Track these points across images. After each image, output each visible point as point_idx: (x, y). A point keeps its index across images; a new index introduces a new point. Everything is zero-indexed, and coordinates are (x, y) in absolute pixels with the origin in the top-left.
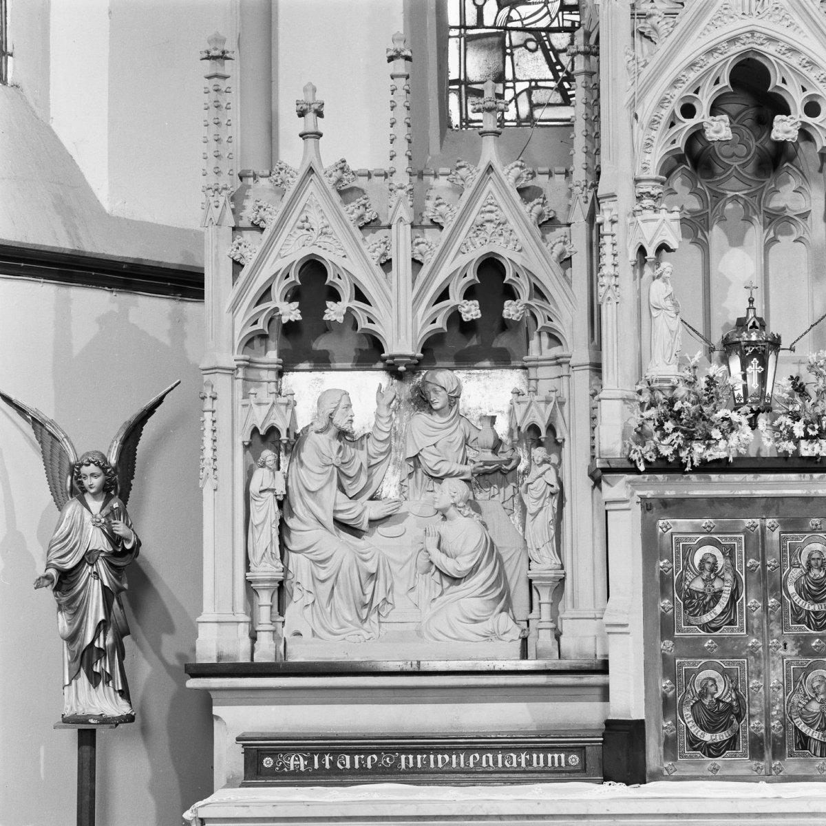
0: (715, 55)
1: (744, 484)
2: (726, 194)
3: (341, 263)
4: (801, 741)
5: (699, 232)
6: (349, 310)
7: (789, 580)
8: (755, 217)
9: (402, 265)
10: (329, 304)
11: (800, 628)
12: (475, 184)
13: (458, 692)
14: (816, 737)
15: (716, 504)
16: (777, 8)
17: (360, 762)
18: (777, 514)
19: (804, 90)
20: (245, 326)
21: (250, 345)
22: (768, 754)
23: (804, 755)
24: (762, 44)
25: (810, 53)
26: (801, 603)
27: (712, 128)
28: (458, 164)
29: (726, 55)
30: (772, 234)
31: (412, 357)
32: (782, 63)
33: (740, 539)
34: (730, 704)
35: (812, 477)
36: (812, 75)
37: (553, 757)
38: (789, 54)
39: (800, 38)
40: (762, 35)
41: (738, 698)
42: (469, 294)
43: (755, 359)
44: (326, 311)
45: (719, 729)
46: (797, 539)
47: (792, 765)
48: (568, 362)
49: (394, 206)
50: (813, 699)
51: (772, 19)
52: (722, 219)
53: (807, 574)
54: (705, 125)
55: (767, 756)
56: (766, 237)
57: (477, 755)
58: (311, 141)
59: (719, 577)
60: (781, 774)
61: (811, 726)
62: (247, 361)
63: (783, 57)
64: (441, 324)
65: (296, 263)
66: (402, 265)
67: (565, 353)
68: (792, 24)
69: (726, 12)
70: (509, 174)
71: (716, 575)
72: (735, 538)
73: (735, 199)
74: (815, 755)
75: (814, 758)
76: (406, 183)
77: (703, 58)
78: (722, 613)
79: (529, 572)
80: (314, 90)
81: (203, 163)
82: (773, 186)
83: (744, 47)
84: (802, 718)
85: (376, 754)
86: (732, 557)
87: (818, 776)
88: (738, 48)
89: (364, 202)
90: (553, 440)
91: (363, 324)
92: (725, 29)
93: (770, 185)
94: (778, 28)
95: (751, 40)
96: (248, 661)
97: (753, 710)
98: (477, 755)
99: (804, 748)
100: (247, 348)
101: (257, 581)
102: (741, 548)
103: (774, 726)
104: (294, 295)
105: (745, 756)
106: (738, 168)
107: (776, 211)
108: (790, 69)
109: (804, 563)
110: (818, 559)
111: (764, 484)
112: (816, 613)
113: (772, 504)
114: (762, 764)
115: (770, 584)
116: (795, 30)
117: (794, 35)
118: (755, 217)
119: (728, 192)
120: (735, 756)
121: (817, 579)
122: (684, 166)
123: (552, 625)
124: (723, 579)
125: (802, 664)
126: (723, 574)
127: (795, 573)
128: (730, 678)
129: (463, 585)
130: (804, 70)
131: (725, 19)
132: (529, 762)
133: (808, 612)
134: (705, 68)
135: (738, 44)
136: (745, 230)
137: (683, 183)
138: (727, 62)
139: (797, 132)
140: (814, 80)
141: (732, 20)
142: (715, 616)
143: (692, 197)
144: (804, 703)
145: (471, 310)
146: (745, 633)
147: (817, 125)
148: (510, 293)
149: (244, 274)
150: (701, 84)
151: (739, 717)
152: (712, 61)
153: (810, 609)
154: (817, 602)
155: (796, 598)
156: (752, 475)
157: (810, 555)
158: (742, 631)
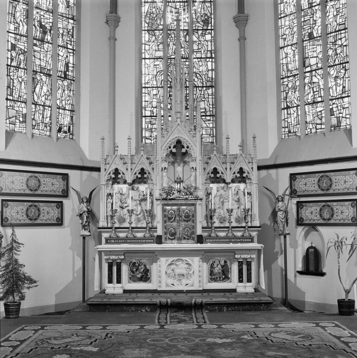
3: (246, 168)
36: (187, 143)
42: (238, 173)
64: (234, 177)
66: (129, 169)
88: (177, 139)
91: (222, 177)
127: (184, 214)
145: (212, 176)
149: (232, 170)
151: (176, 235)
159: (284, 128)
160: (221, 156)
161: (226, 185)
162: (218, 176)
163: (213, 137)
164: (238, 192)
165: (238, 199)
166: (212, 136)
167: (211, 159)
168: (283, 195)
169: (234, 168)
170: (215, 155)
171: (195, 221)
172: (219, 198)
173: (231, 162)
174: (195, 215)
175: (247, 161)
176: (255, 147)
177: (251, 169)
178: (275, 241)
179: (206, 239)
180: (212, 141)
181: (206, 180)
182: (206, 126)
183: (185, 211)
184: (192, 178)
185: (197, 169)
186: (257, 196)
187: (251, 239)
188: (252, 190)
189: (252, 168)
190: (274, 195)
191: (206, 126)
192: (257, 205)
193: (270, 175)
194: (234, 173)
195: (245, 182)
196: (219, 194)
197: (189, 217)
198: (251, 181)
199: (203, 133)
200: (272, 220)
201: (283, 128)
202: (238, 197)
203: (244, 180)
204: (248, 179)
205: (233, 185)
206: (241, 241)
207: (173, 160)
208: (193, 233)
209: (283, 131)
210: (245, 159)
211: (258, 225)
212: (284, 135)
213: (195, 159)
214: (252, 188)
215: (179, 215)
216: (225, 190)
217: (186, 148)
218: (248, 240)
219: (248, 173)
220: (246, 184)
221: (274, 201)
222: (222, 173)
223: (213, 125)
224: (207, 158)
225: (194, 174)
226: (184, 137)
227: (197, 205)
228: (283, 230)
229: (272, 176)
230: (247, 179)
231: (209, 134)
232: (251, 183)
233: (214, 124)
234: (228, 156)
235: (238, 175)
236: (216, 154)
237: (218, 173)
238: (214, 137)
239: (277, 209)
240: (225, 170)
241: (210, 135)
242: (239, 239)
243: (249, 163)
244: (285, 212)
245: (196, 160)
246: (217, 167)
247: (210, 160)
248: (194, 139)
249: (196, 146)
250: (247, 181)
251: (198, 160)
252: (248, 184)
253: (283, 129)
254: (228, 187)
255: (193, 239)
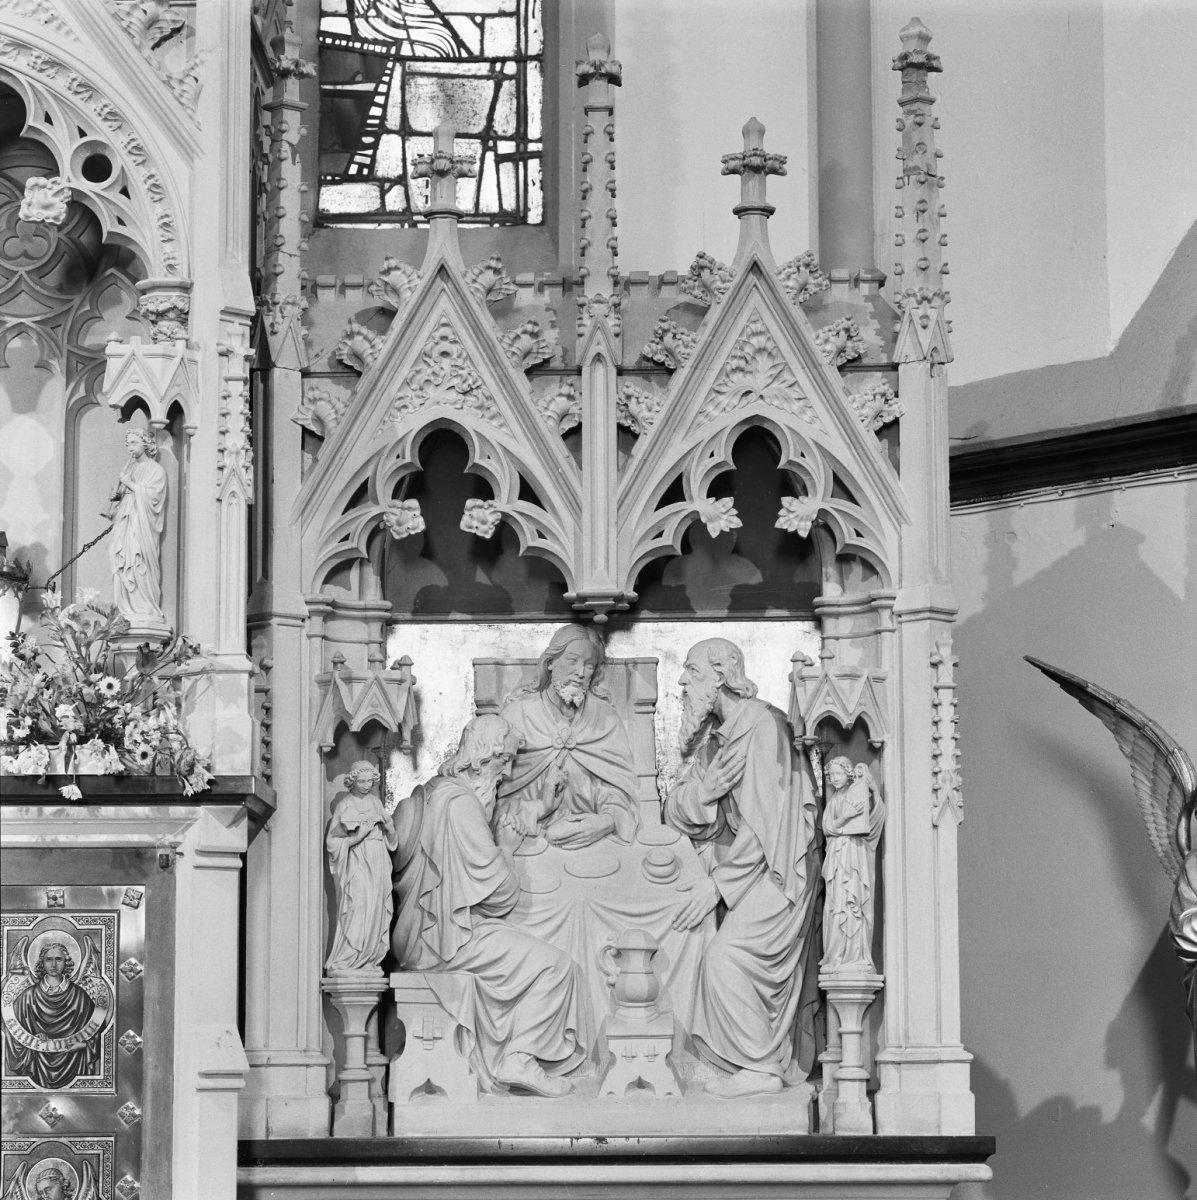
2: (5, 322)
3: (809, 433)
6: (822, 512)
8: (54, 362)
9: (600, 439)
10: (786, 501)
11: (20, 1083)
19: (82, 134)
21: (339, 578)
25: (82, 68)
26: (23, 1037)
28: (385, 266)
30: (82, 392)
31: (619, 598)
35: (40, 813)
36: (90, 109)
38: (51, 71)
39: (66, 43)
42: (717, 489)
46: (23, 923)
48: (891, 607)
49: (587, 335)
51: (19, 10)
53: (37, 985)
62: (328, 604)
64: (671, 539)
65: (728, 430)
66: (600, 439)
67: (885, 592)
68: (53, 18)
73: (20, 330)
80: (761, 132)
82: (88, 308)
89: (847, 324)
91: (528, 539)
93: (81, 305)
96: (324, 1135)
100: (328, 586)
104: (411, 486)
106: (26, 276)
107: (92, 351)
108: (55, 97)
109: (32, 967)
112: (50, 1056)
118: (54, 362)
119: (6, 318)
123: (864, 1074)
125: (20, 1148)
127: (15, 985)
129: (519, 1007)
130: (76, 100)
133: (35, 1055)
136: (41, 385)
140: (93, 115)
145: (409, 519)
148: (791, 484)
149: (640, 448)
153: (40, 1050)
154: (52, 1036)
157: (43, 952)
161: (578, 642)
162: (478, 519)
163: (520, 157)
164: (715, 717)
165: (723, 801)
166: (506, 147)
167: (398, 323)
169: (671, 421)
170: (442, 271)
171: (151, 1075)
172: (484, 786)
173: (631, 361)
174: (151, 990)
175: (824, 344)
176: (930, 179)
180: (509, 204)
182: (447, 46)
184: (134, 534)
185: (192, 418)
189: (889, 430)
191: (447, 46)
193: (1128, 539)
194: (675, 493)
195: (805, 605)
196: (491, 737)
197: (81, 1019)
198: (872, 588)
199: (416, 124)
200: (1140, 1054)
202: (715, 779)
203: (800, 576)
205: (666, 644)
211: (960, 1122)
213: (174, 298)
214: (887, 668)
216: (568, 692)
219: (842, 487)
220: (818, 622)
222: (528, 492)
225: (149, 479)
226: (49, 32)
227: (183, 869)
229: (1145, 553)
230: (830, 570)
231: (479, 126)
235: (722, 517)
236: (456, 265)
238: (534, 165)
240: (560, 449)
243: (851, 365)
245: (183, 317)
246: (468, 420)
247: (383, 331)
248: (174, 57)
249: (188, 151)
251: (205, 323)
254: (599, 662)
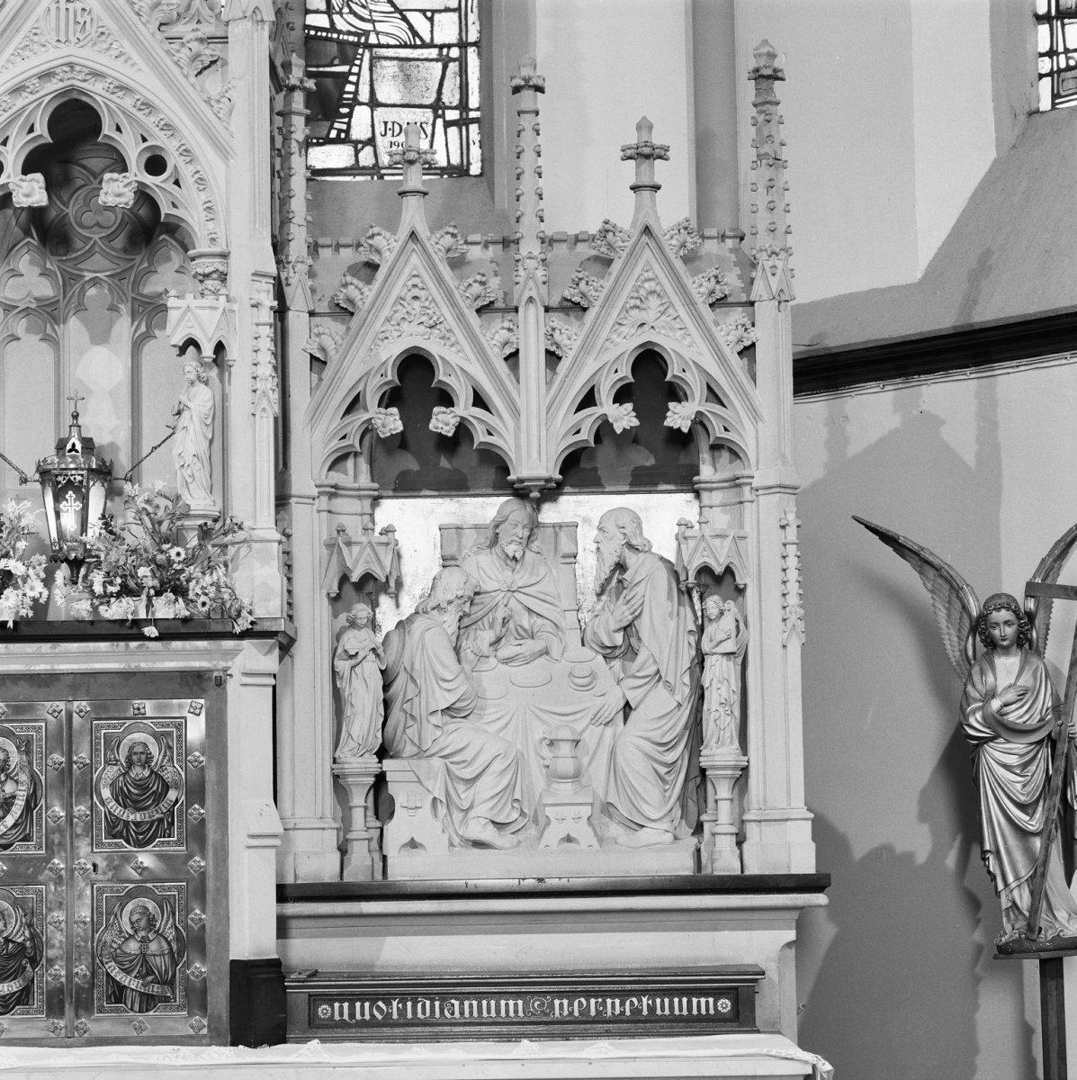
0: (24, 94)
1: (41, 657)
4: (114, 992)
5: (48, 326)
7: (103, 782)
8: (122, 306)
9: (533, 360)
10: (672, 405)
11: (116, 844)
12: (392, 259)
13: (710, 915)
14: (133, 987)
15: (8, 683)
16: (103, 33)
17: (597, 1009)
18: (87, 695)
20: (566, 434)
22: (69, 1010)
23: (117, 1010)
24: (85, 81)
27: (21, 191)
29: (38, 95)
30: (143, 328)
31: (548, 480)
32: (112, 106)
33: (40, 728)
34: (22, 945)
35: (127, 646)
36: (150, 121)
37: (699, 1002)
38: (120, 94)
40: (84, 69)
41: (33, 937)
42: (621, 396)
43: (70, 492)
44: (669, 414)
45: (8, 976)
47: (97, 1024)
50: (131, 936)
51: (96, 48)
52: (81, 308)
53: (127, 773)
54: (11, 187)
55: (67, 1012)
56: (136, 331)
57: (634, 1000)
58: (646, 194)
59: (12, 779)
60: (86, 1035)
61: (128, 972)
62: (332, 487)
63: (113, 97)
64: (586, 435)
66: (533, 360)
67: (746, 473)
68: (122, 54)
69: (36, 38)
70: (440, 244)
71: (8, 776)
72: (34, 727)
74: (132, 1009)
75: (132, 1013)
76: (536, 252)
77: (5, 98)
78: (15, 826)
79: (334, 766)
80: (650, 128)
81: (789, 219)
83: (61, 85)
84: (116, 962)
85: (457, 999)
86: (28, 752)
87: (134, 1037)
88: (54, 86)
90: (733, 587)
91: (480, 437)
92: (34, 61)
93: (141, 263)
94: (103, 59)
95: (70, 75)
96: (337, 880)
97: (51, 953)
98: (583, 1000)
99: (118, 1001)
101: (714, 768)
102: (40, 740)
103: (77, 973)
104: (391, 398)
105: (41, 1012)
107: (149, 297)
110: (142, 753)
111: (66, 657)
112: (137, 824)
113: (80, 683)
114: (62, 1023)
115: (74, 783)
116: (126, 61)
117: (126, 69)
118: (122, 306)
120: (28, 1013)
121: (140, 780)
122: (29, 239)
124: (17, 782)
125: (118, 891)
126: (17, 774)
127: (112, 772)
128: (23, 910)
130: (140, 115)
131: (36, 47)
132: (402, 1012)
133: (126, 823)
134: (11, 112)
135: (55, 81)
136: (111, 324)
137: (32, 262)
138: (41, 103)
139: (132, 195)
140: (153, 127)
141: (43, 49)
142: (5, 830)
143: (43, 280)
144: (119, 942)
145: (391, 422)
146: (44, 852)
147: (157, 186)
148: (675, 393)
149: (563, 367)
150: (9, 134)
151: (34, 962)
152: (20, 103)
154: (139, 810)
155: (112, 804)
156: (49, 645)
157: (131, 748)
158: (41, 847)
159: (1045, 18)
160: (475, 253)
161: (518, 512)
162: (443, 421)
166: (452, 115)
167: (380, 275)
168: (1031, 588)
169: (586, 348)
171: (212, 836)
172: (450, 620)
174: (211, 776)
175: (699, 288)
176: (776, 162)
177: (738, 364)
178: (976, 1007)
179: (314, 1000)
180: (455, 160)
181: (338, 461)
182: (405, 36)
183: (126, 742)
184: (191, 440)
185: (232, 353)
186: (793, 600)
187: (733, 993)
188: (750, 545)
189: (748, 351)
190: (954, 588)
191: (405, 36)
192: (795, 680)
195: (686, 481)
196: (454, 584)
199: (381, 98)
201: (1040, 19)
202: (622, 613)
204: (716, 447)
205: (583, 511)
206: (636, 1011)
207: (45, 289)
208: (193, 942)
209: (1044, 46)
210: (688, 281)
212: (1047, 82)
213: (217, 264)
214: (749, 528)
215: (65, 773)
216: (511, 549)
217: (137, 173)
218: (703, 1004)
219: (713, 395)
220: (697, 494)
221: (954, 654)
222: (479, 401)
223: (463, 26)
224: (353, 270)
225: (201, 400)
227: (232, 687)
228: (1034, 910)
230: (705, 456)
231: (431, 99)
232: (735, 483)
233: (472, 17)
234: (530, 247)
235: (624, 418)
236: (423, 232)
237: (446, 399)
238: (474, 128)
239: (975, 720)
240: (503, 368)
241: (437, 107)
242: (623, 995)
243: (719, 303)
244: (1052, 741)
245: (223, 277)
246: (434, 347)
247: (369, 281)
248: (212, 82)
249: (224, 152)
250: (706, 472)
251: (239, 270)
252: (717, 497)
253: (1044, 29)
254: (534, 526)
255: (197, 998)
